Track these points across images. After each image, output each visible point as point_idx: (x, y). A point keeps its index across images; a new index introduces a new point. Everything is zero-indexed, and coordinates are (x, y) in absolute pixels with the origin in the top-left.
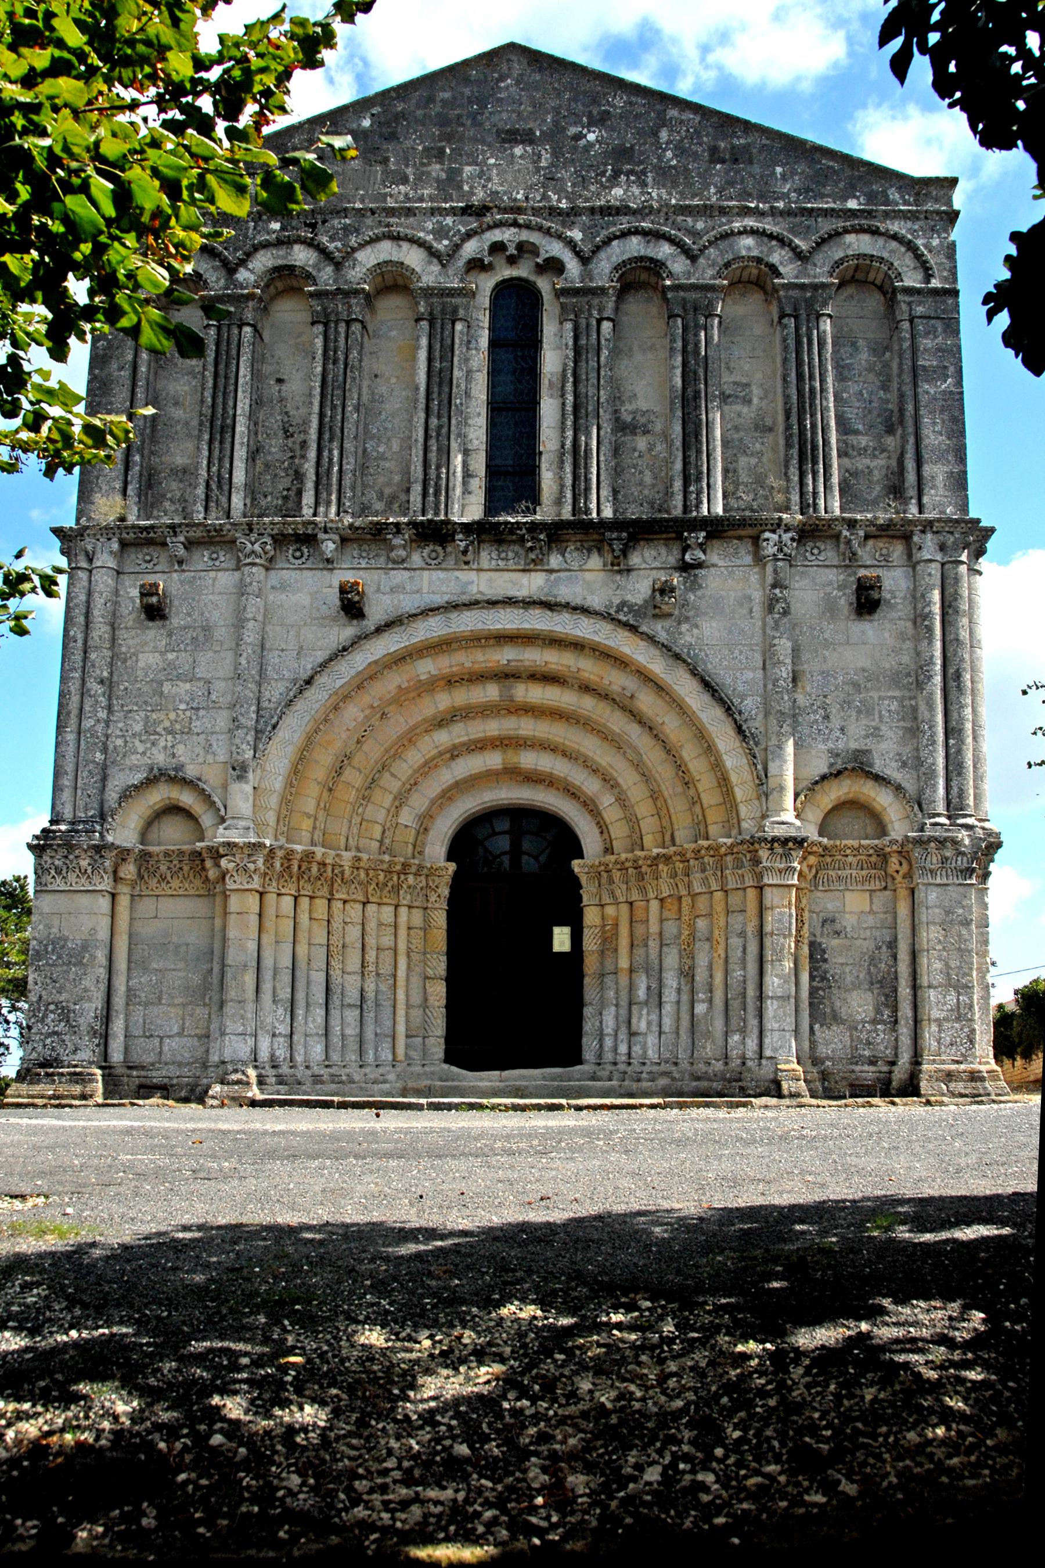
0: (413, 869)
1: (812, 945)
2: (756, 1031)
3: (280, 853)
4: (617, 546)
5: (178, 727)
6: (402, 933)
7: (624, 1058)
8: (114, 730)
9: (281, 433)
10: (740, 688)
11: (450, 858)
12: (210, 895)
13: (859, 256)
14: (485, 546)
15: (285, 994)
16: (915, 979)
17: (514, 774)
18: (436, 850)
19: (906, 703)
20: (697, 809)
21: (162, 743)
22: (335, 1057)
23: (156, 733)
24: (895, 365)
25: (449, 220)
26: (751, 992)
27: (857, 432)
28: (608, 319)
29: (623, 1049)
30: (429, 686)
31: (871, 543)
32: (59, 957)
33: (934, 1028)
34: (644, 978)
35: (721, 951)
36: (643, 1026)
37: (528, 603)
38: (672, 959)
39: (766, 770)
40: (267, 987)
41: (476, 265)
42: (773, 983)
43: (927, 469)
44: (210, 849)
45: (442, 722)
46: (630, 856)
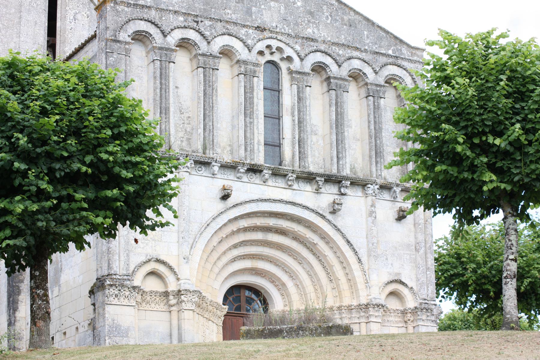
25: (251, 31)
32: (119, 333)
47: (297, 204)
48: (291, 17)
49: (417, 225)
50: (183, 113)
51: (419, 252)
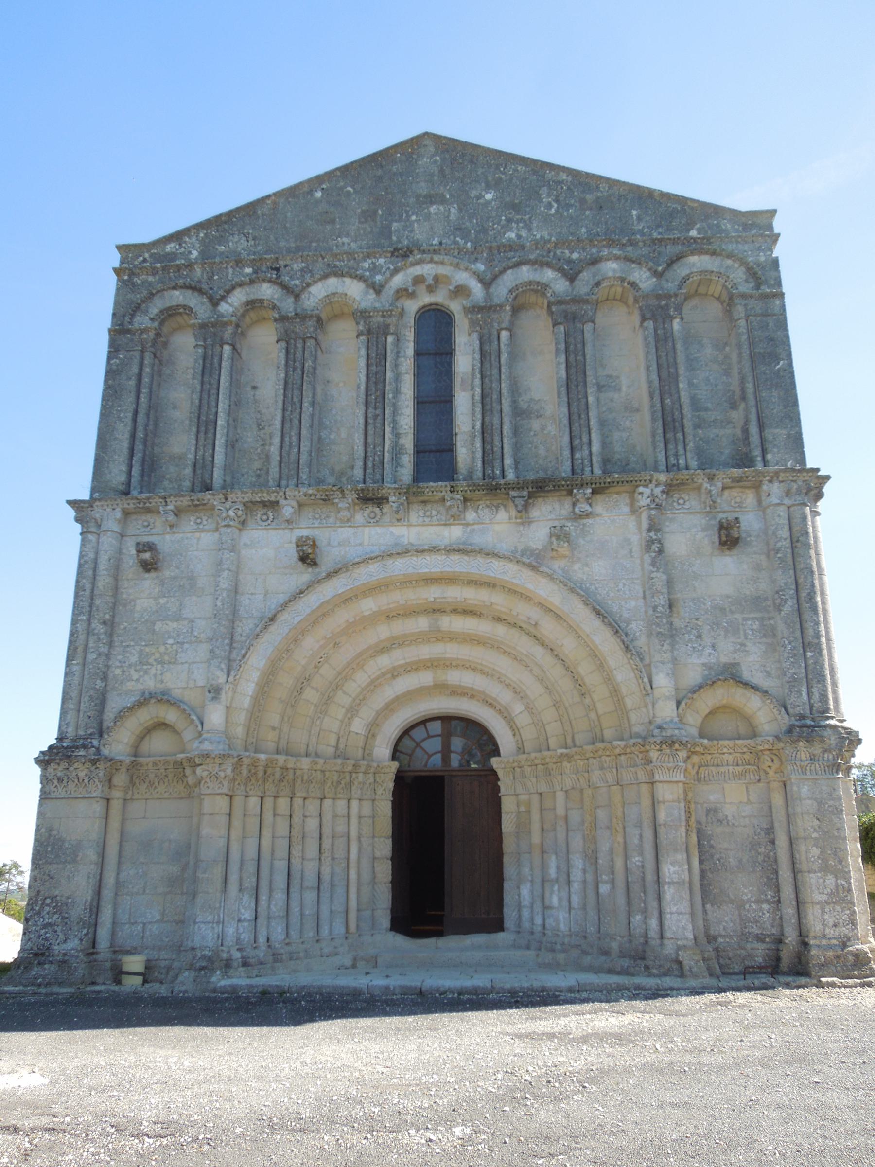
0: (363, 769)
1: (699, 832)
2: (656, 913)
3: (246, 761)
4: (520, 502)
5: (166, 658)
6: (354, 821)
7: (540, 929)
8: (114, 662)
9: (255, 427)
10: (626, 615)
11: (394, 758)
12: (189, 797)
13: (702, 272)
14: (415, 506)
15: (250, 882)
16: (793, 863)
17: (440, 688)
18: (383, 750)
19: (766, 622)
20: (593, 715)
21: (153, 671)
22: (294, 934)
23: (148, 664)
24: (734, 357)
26: (650, 877)
27: (706, 409)
28: (506, 329)
29: (538, 921)
30: (373, 619)
31: (726, 492)
33: (817, 910)
34: (554, 857)
35: (620, 839)
36: (555, 900)
37: (450, 550)
38: (577, 842)
39: (651, 682)
40: (233, 878)
41: (403, 293)
42: (669, 870)
43: (769, 434)
44: (189, 760)
45: (383, 648)
46: (538, 755)
47: (480, 551)
48: (471, 222)
49: (772, 553)
50: (263, 428)
51: (780, 610)
